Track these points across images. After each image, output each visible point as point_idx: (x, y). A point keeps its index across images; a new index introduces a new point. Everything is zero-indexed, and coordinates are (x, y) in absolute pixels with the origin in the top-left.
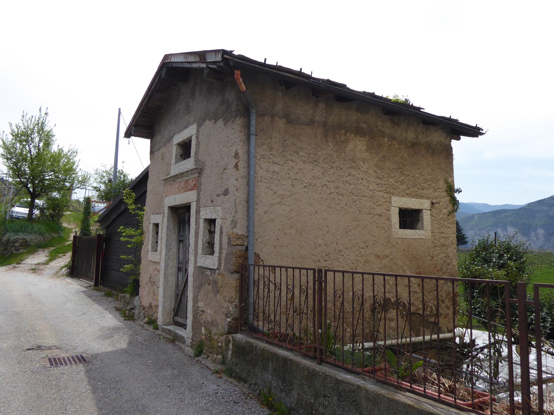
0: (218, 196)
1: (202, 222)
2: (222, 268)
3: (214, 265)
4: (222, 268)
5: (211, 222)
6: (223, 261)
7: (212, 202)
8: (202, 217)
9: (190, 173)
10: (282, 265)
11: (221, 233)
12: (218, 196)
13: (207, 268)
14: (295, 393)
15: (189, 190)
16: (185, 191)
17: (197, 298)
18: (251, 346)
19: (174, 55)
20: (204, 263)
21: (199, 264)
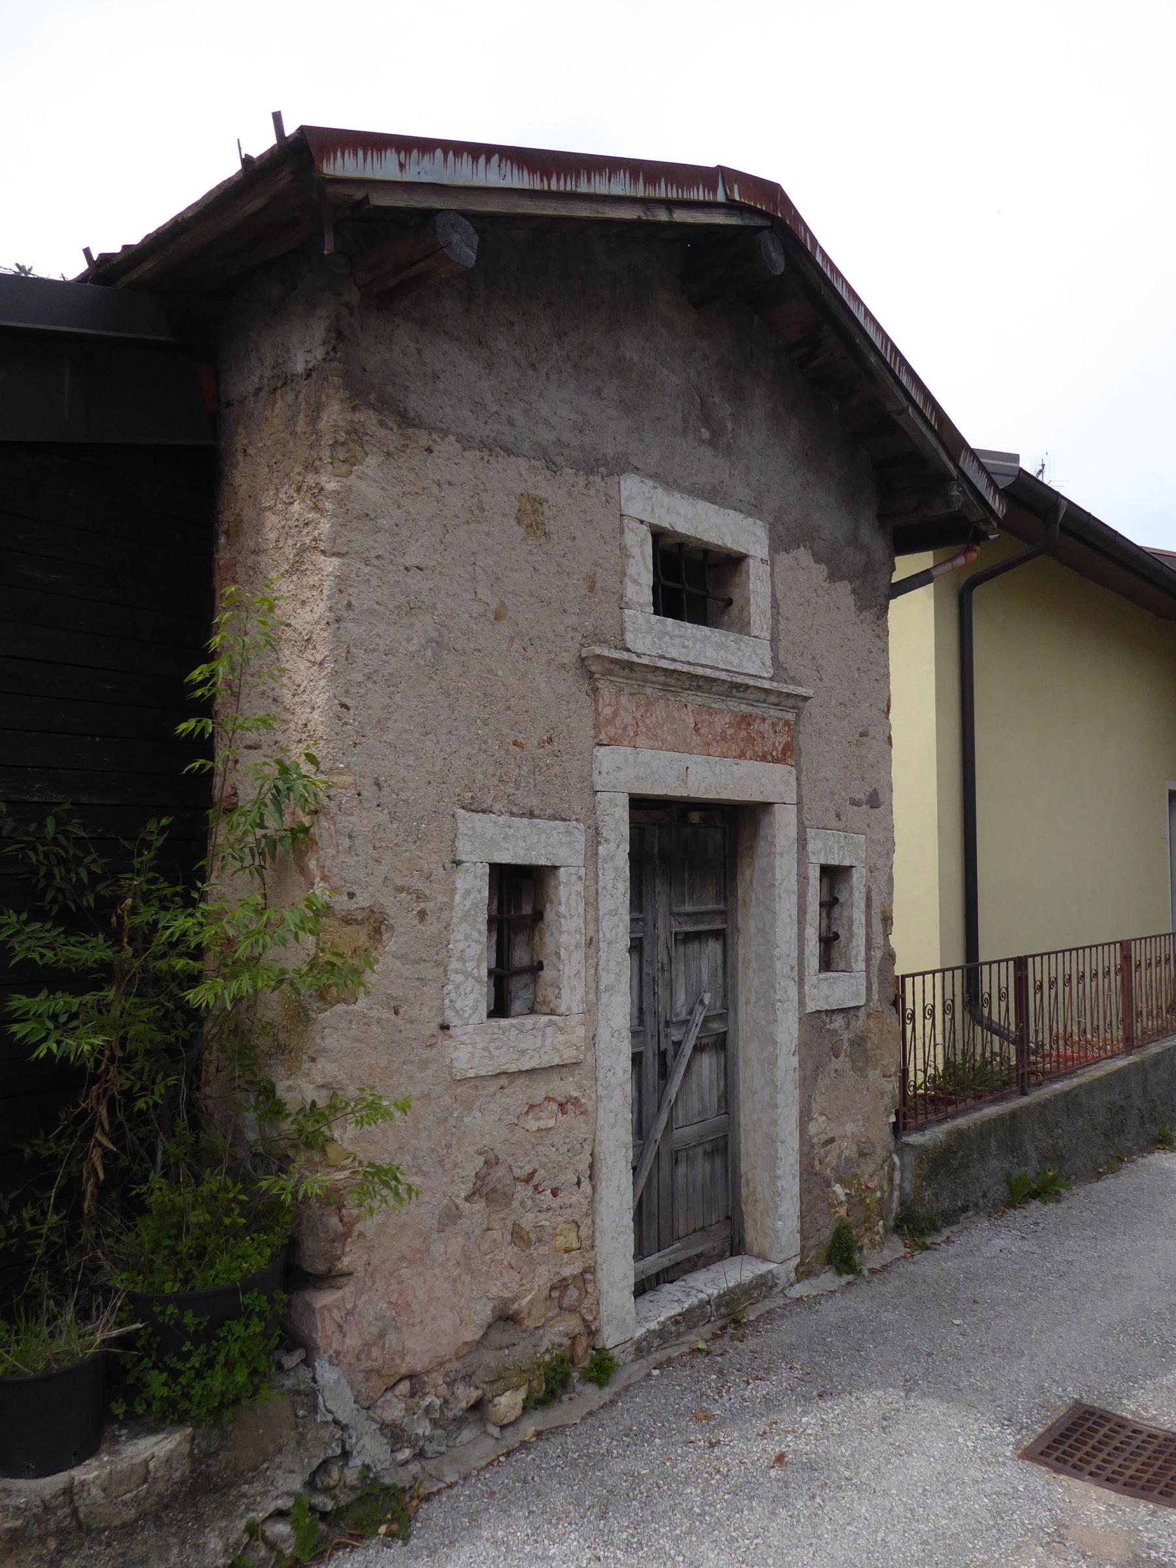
0: (855, 803)
1: (814, 874)
2: (875, 997)
3: (857, 995)
4: (875, 997)
5: (833, 875)
6: (875, 980)
7: (838, 816)
8: (813, 859)
9: (772, 699)
10: (998, 958)
11: (868, 906)
12: (855, 803)
13: (833, 1011)
14: (1032, 1153)
15: (763, 758)
16: (742, 755)
17: (810, 1111)
18: (960, 1134)
19: (844, 280)
20: (827, 997)
21: (811, 1007)
